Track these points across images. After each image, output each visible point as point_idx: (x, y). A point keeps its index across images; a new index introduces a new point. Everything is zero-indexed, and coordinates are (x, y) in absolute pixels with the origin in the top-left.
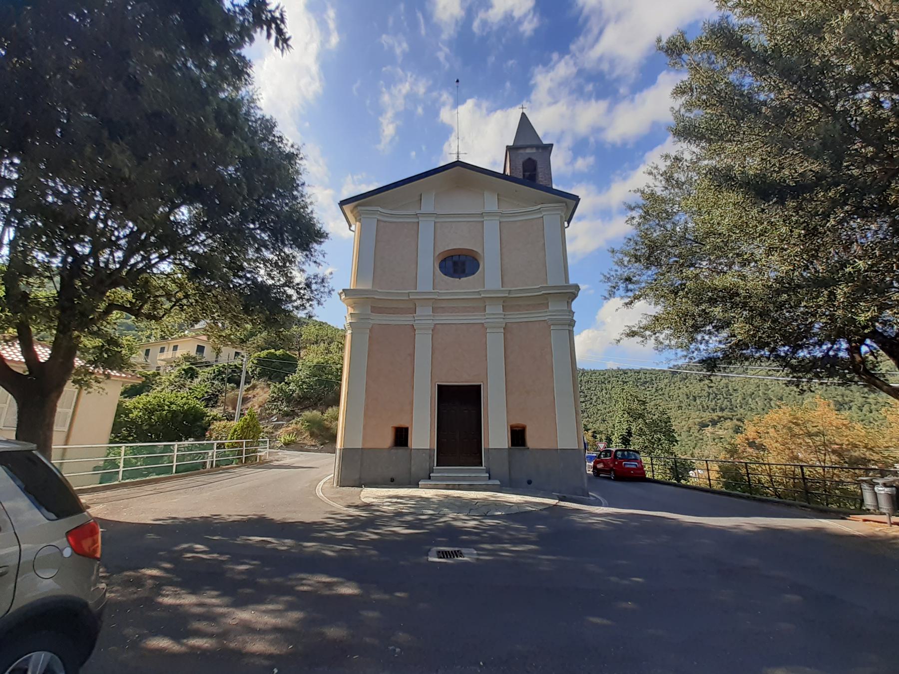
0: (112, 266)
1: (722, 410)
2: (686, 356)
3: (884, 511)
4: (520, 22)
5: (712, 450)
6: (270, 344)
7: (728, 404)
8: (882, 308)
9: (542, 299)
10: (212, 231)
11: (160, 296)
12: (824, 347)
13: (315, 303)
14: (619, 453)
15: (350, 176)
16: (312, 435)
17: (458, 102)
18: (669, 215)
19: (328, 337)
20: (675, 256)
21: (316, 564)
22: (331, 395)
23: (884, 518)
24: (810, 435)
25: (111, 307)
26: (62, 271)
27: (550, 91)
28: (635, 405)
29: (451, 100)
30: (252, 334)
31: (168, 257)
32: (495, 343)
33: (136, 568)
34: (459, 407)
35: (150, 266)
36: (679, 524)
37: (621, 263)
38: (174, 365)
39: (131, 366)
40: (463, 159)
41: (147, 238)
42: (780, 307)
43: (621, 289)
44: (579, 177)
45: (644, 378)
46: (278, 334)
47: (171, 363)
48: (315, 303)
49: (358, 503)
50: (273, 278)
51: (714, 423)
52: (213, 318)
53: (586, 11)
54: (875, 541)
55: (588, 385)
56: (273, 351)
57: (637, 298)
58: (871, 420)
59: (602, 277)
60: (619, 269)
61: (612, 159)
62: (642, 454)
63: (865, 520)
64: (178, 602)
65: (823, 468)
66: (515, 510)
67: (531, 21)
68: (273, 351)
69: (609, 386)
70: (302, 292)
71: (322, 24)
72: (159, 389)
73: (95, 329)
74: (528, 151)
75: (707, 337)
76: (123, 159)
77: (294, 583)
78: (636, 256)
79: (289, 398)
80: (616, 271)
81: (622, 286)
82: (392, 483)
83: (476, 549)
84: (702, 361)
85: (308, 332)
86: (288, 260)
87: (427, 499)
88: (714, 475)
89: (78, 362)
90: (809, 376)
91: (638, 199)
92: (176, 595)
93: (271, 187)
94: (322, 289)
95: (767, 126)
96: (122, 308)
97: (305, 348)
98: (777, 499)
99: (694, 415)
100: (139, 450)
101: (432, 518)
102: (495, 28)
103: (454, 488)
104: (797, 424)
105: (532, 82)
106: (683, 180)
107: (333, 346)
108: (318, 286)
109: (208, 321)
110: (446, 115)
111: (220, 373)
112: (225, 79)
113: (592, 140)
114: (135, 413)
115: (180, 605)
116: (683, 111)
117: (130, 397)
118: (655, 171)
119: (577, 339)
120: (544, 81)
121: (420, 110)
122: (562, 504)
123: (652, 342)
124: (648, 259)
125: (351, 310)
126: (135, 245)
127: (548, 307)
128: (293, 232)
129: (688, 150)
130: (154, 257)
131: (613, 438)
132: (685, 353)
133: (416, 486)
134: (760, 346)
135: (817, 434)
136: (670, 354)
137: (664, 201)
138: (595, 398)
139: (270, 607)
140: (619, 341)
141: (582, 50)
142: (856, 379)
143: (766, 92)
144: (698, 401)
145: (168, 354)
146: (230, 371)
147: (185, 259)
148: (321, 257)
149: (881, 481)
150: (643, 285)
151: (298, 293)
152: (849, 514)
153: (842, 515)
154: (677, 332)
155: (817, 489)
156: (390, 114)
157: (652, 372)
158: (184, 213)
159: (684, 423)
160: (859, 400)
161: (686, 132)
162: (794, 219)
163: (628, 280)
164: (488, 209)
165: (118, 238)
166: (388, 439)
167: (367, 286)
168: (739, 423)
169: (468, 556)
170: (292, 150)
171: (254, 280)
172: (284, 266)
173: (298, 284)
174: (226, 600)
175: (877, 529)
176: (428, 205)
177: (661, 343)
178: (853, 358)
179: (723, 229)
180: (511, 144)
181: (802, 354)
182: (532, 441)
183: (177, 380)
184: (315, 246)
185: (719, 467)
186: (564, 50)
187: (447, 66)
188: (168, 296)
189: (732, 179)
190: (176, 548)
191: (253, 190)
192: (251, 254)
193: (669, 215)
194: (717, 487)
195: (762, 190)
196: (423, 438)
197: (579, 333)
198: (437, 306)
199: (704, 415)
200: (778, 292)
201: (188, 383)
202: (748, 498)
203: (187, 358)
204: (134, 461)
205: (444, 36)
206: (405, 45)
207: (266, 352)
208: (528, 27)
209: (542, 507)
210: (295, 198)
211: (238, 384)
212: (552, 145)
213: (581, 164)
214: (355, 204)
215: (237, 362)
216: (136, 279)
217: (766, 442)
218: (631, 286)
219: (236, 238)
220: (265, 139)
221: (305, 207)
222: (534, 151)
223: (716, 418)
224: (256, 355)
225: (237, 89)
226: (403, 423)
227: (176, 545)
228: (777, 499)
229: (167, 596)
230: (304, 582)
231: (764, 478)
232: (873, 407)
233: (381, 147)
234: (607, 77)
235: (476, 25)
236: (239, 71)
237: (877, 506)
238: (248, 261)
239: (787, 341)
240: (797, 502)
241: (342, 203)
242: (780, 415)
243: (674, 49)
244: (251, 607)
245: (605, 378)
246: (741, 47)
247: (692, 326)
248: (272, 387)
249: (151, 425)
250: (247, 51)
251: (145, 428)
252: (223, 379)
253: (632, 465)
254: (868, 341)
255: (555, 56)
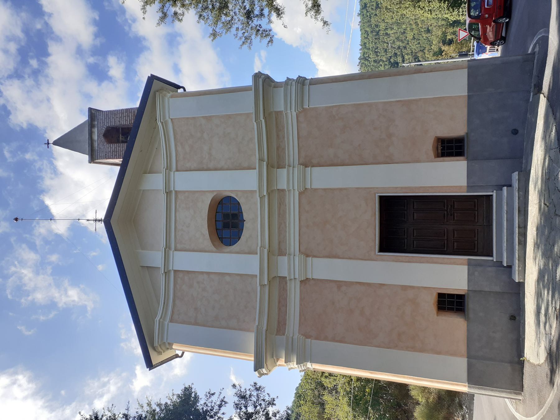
9: (272, 121)
14: (472, 14)
37: (228, 25)
40: (102, 215)
43: (259, 22)
48: (271, 410)
49: (546, 369)
55: (383, 57)
60: (235, 26)
69: (382, 26)
74: (95, 137)
78: (221, 9)
80: (237, 29)
81: (256, 22)
82: (517, 318)
87: (541, 275)
94: (254, 399)
107: (327, 382)
110: (60, 228)
113: (91, 60)
119: (321, 75)
121: (54, 258)
125: (282, 361)
127: (281, 112)
131: (452, 19)
138: (398, 43)
140: (325, 23)
148: (214, 398)
156: (55, 294)
163: (249, 15)
164: (160, 185)
166: (455, 324)
167: (250, 339)
176: (156, 258)
182: (457, 127)
184: (200, 405)
196: (452, 273)
197: (314, 67)
198: (276, 249)
209: (551, 114)
218: (257, 12)
222: (95, 130)
226: (431, 302)
233: (90, 306)
234: (23, 44)
241: (150, 365)
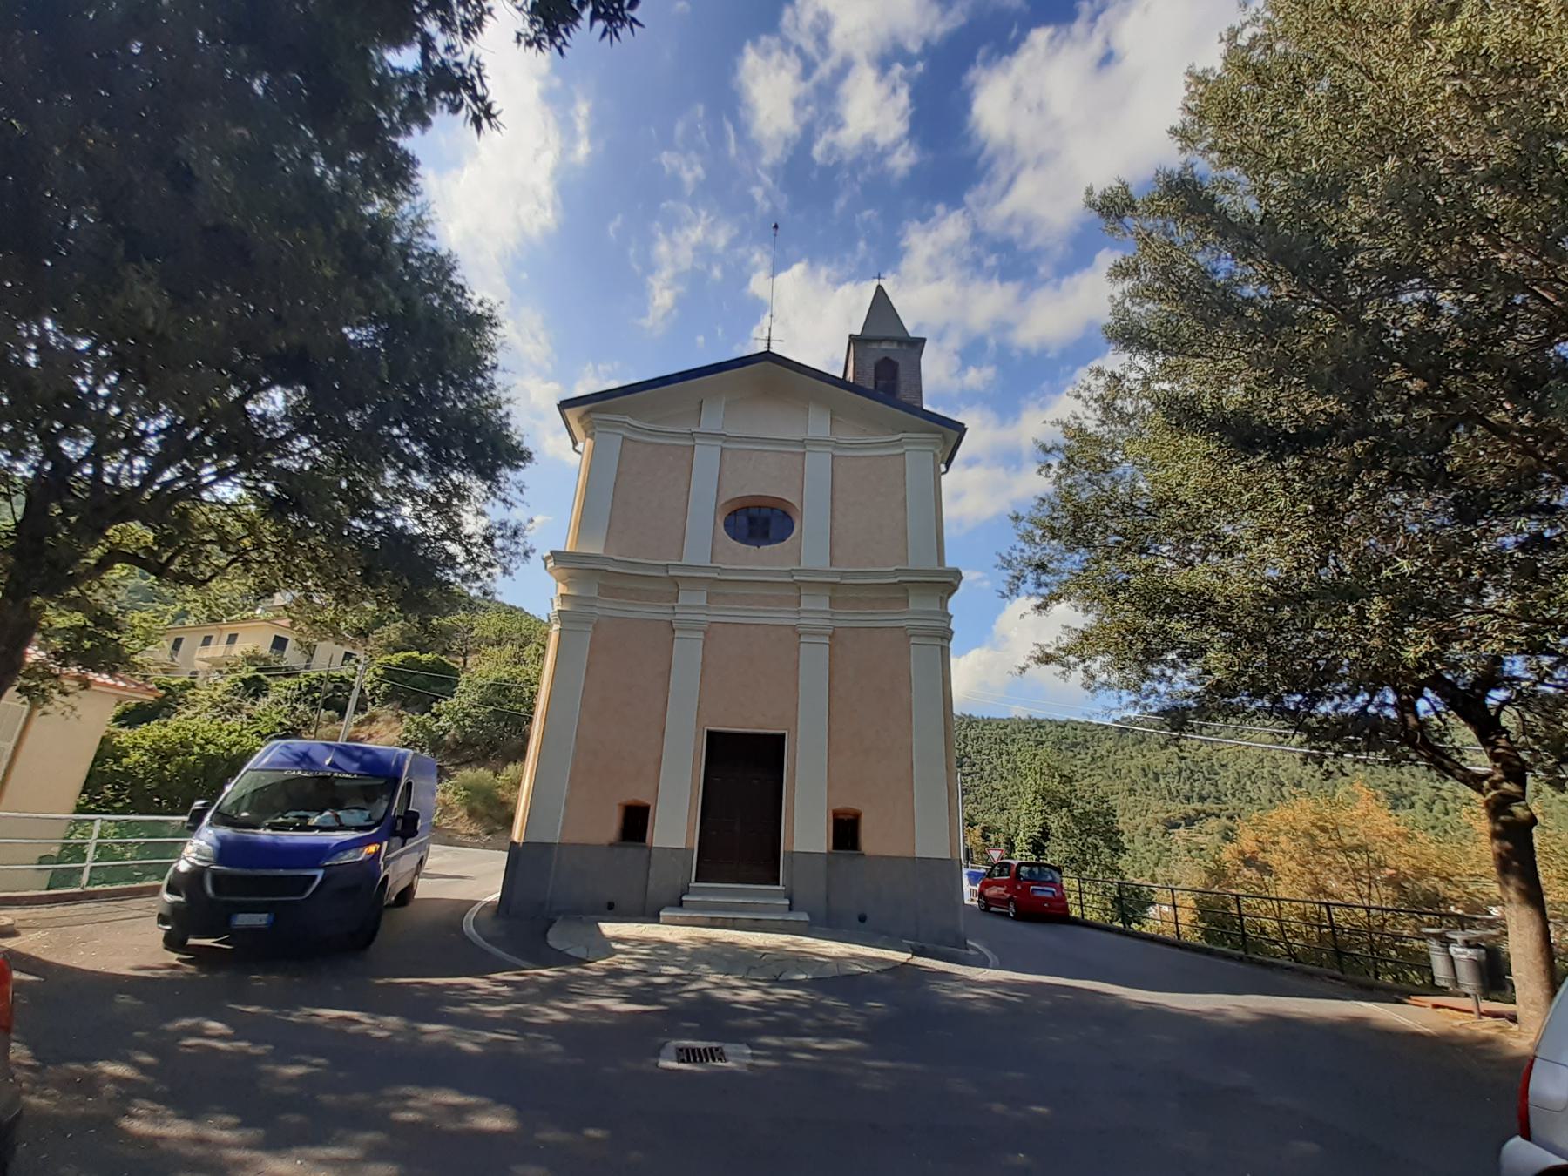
0: (125, 483)
1: (1202, 799)
2: (1136, 703)
3: (1468, 991)
4: (885, 153)
5: (1191, 875)
6: (411, 642)
7: (1212, 788)
8: (1444, 640)
9: (900, 589)
10: (323, 437)
11: (211, 542)
12: (1359, 699)
13: (497, 570)
15: (590, 365)
16: (472, 814)
17: (779, 266)
18: (1107, 466)
19: (521, 634)
20: (1116, 533)
21: (441, 1067)
22: (516, 740)
23: (1468, 1003)
24: (1346, 850)
25: (115, 555)
26: (30, 488)
27: (931, 261)
28: (1054, 784)
29: (767, 261)
30: (380, 622)
31: (234, 474)
32: (814, 660)
33: (88, 1059)
34: (745, 771)
35: (199, 487)
36: (1120, 1005)
37: (1029, 538)
38: (225, 669)
39: (134, 666)
40: (776, 349)
41: (199, 438)
42: (1279, 629)
44: (970, 398)
45: (1074, 738)
46: (424, 623)
47: (218, 666)
48: (497, 570)
50: (424, 524)
51: (1190, 821)
52: (306, 588)
53: (990, 148)
54: (1453, 1045)
55: (974, 746)
56: (415, 654)
57: (1057, 598)
58: (1448, 827)
59: (998, 561)
60: (1026, 548)
61: (1022, 375)
62: (1067, 872)
63: (1436, 1006)
64: (159, 1131)
65: (1368, 909)
66: (833, 970)
67: (904, 154)
68: (415, 654)
70: (475, 550)
71: (566, 126)
72: (189, 713)
73: (74, 592)
74: (885, 346)
75: (1169, 672)
76: (145, 295)
77: (391, 1104)
78: (1052, 528)
79: (436, 744)
80: (1023, 551)
81: (1030, 576)
83: (751, 1046)
84: (1163, 712)
85: (486, 624)
86: (459, 492)
87: (671, 946)
88: (1186, 916)
89: (34, 654)
90: (1337, 747)
91: (1057, 436)
92: (155, 1118)
93: (436, 368)
94: (513, 548)
95: (1252, 339)
96: (132, 559)
97: (477, 651)
98: (1292, 963)
99: (1155, 805)
100: (131, 829)
101: (676, 983)
102: (848, 158)
103: (724, 925)
104: (1324, 830)
105: (904, 243)
106: (1130, 410)
107: (529, 651)
108: (507, 543)
109: (297, 594)
110: (758, 284)
111: (311, 689)
112: (368, 182)
113: (992, 342)
114: (135, 756)
115: (162, 1138)
116: (1128, 304)
117: (132, 725)
118: (1085, 394)
120: (921, 244)
121: (717, 273)
122: (918, 961)
123: (1077, 675)
124: (1073, 533)
125: (562, 589)
126: (176, 446)
128: (468, 445)
129: (1131, 365)
130: (208, 473)
131: (1017, 842)
132: (1133, 698)
133: (655, 918)
134: (1258, 694)
135: (1358, 848)
136: (1108, 699)
137: (1099, 442)
138: (988, 768)
139: (334, 1152)
140: (1023, 669)
141: (982, 203)
142: (1413, 756)
143: (1254, 286)
144: (1162, 782)
145: (217, 650)
146: (330, 686)
147: (266, 480)
148: (515, 492)
149: (1459, 936)
150: (1065, 577)
151: (468, 552)
152: (1409, 994)
153: (1397, 995)
154: (1120, 663)
155: (1358, 945)
156: (666, 273)
157: (1086, 726)
158: (274, 401)
159: (1138, 819)
160: (1426, 792)
161: (1128, 336)
162: (1297, 486)
163: (1041, 567)
164: (811, 434)
165: (145, 434)
166: (610, 828)
168: (1230, 824)
169: (736, 1059)
170: (480, 310)
171: (388, 525)
172: (449, 504)
173: (470, 537)
174: (251, 1134)
175: (1457, 1023)
176: (712, 420)
177: (1093, 677)
178: (1404, 720)
179: (1186, 495)
180: (858, 332)
181: (1325, 708)
182: (871, 840)
183: (226, 698)
185: (1196, 901)
186: (955, 202)
187: (767, 206)
188: (223, 540)
189: (1199, 416)
190: (170, 1027)
191: (413, 371)
192: (390, 478)
193: (1107, 466)
194: (1193, 937)
195: (1244, 436)
196: (676, 826)
197: (963, 652)
199: (1172, 806)
200: (1276, 604)
201: (247, 705)
202: (1241, 959)
203: (251, 659)
204: (120, 850)
205: (766, 160)
206: (699, 170)
207: (402, 655)
208: (902, 161)
210: (479, 390)
211: (342, 711)
212: (924, 340)
213: (973, 377)
214: (586, 409)
215: (346, 671)
216: (170, 511)
217: (1273, 859)
218: (1044, 578)
219: (369, 451)
220: (435, 288)
221: (497, 405)
222: (894, 346)
223: (1192, 813)
224: (383, 660)
225: (396, 203)
226: (640, 796)
227: (171, 1019)
228: (1292, 963)
229: (139, 1118)
230: (411, 1103)
231: (1271, 925)
232: (1450, 805)
233: (647, 322)
235: (818, 150)
236: (397, 172)
237: (1455, 981)
238: (383, 490)
239: (1294, 684)
240: (1325, 970)
241: (564, 405)
242: (1300, 812)
243: (1113, 207)
244: (296, 1151)
245: (1004, 733)
246: (1213, 212)
247: (1145, 654)
248: (406, 720)
249: (162, 782)
250: (412, 142)
251: (148, 786)
252: (314, 701)
253: (1047, 892)
254: (1428, 693)
255: (940, 209)
